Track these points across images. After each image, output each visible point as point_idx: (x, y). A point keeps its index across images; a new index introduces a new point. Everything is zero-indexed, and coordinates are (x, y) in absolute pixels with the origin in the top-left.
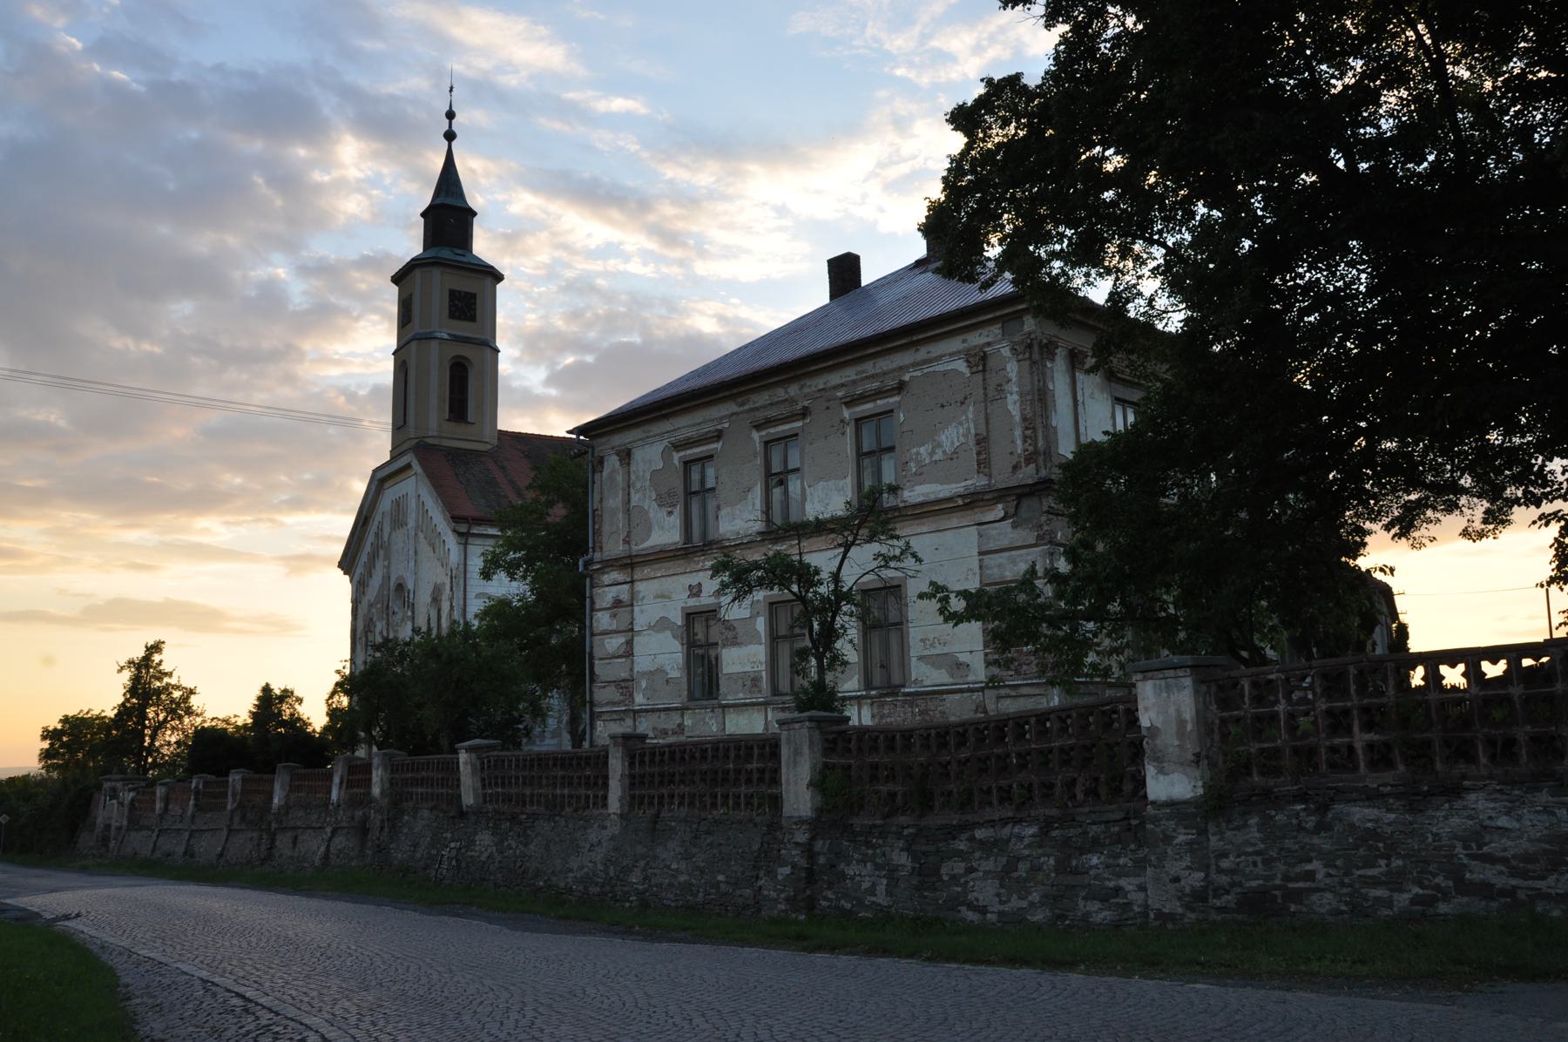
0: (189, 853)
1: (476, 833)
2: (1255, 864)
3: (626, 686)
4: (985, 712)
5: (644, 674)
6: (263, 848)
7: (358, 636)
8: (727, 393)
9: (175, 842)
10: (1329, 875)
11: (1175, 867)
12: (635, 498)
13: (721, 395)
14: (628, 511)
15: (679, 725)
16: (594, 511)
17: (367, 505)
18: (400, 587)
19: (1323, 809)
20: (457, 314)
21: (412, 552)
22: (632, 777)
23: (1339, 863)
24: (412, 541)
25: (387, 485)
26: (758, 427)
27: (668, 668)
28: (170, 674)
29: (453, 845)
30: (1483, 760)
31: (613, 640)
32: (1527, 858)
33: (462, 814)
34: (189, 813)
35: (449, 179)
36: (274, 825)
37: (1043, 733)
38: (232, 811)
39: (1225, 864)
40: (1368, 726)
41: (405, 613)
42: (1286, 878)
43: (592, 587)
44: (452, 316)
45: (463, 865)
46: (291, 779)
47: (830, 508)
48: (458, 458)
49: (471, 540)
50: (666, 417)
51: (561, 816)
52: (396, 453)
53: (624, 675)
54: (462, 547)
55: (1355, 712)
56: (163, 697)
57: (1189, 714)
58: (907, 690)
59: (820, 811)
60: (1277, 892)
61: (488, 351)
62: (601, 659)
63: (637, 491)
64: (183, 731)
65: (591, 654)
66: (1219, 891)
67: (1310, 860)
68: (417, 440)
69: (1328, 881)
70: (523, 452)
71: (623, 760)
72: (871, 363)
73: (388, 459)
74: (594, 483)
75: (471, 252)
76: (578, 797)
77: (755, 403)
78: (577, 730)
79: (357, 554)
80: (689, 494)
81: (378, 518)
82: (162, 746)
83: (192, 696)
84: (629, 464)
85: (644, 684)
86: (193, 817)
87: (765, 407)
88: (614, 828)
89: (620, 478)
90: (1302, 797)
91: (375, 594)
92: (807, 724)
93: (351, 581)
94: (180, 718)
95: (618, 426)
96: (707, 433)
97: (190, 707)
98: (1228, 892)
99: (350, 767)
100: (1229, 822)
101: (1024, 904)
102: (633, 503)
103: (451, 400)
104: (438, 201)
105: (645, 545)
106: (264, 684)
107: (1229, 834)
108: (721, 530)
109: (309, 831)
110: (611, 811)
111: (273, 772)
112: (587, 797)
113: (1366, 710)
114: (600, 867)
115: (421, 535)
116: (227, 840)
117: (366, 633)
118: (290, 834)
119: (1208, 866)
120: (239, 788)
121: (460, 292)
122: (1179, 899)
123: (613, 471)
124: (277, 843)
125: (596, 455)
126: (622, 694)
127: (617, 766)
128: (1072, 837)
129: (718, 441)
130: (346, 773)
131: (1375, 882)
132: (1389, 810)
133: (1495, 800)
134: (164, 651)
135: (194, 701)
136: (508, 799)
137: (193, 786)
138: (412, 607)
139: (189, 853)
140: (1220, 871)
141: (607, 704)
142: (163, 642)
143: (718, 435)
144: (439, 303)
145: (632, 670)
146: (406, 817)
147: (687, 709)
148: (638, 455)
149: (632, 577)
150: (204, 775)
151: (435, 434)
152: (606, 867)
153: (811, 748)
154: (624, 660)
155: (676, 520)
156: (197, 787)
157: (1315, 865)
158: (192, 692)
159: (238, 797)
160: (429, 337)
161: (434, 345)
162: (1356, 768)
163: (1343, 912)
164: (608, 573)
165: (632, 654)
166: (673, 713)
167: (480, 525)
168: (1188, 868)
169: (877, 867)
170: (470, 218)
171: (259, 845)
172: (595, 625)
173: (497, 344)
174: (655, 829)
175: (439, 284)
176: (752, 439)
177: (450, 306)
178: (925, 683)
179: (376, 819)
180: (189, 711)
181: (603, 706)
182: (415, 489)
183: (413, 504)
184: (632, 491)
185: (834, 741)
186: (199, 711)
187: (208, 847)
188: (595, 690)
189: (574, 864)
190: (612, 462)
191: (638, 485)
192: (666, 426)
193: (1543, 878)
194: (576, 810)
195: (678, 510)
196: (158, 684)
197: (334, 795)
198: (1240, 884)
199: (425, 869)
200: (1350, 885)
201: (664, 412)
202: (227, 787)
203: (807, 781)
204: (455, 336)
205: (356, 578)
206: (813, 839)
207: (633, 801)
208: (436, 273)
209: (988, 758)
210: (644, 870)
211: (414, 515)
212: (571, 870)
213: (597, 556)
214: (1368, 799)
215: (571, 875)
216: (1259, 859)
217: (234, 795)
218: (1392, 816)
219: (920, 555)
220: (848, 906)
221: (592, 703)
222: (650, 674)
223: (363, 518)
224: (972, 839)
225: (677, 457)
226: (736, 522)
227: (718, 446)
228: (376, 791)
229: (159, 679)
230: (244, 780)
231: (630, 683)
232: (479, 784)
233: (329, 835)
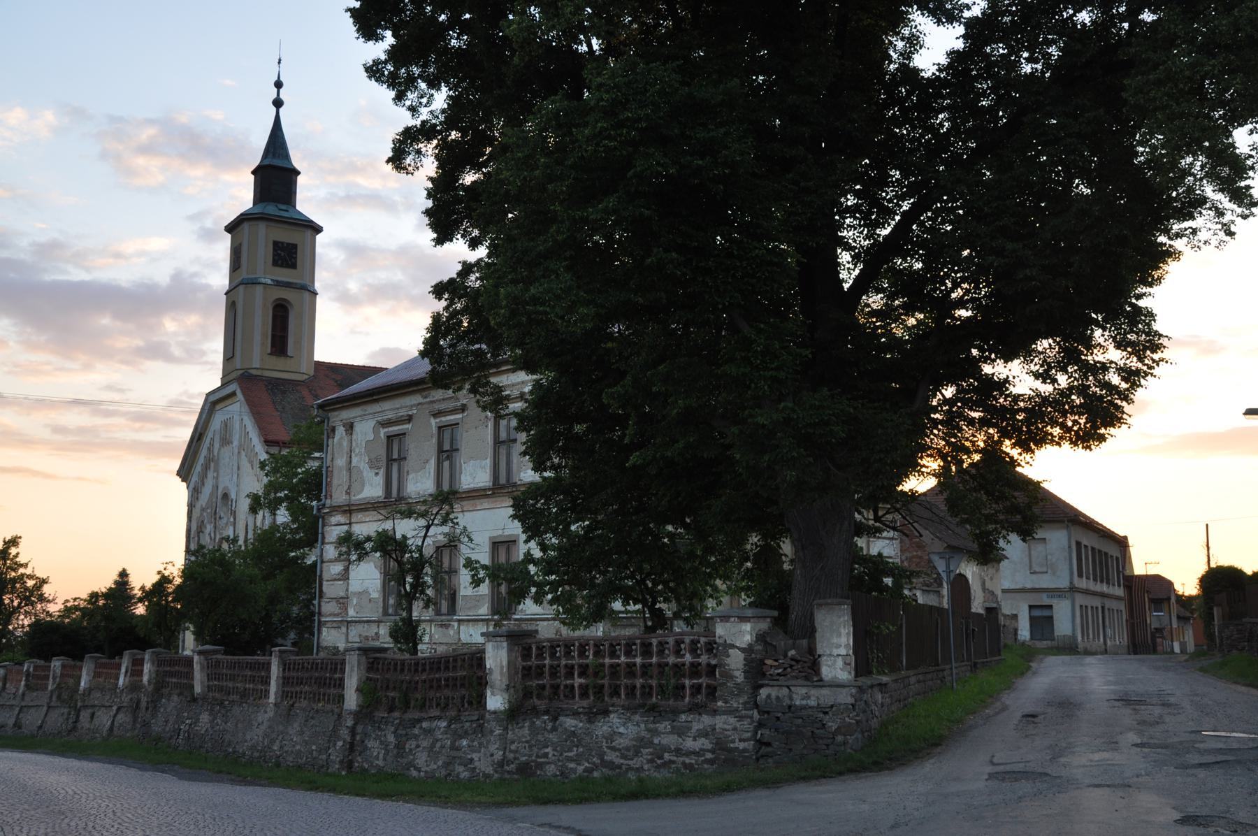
0: (18, 725)
1: (200, 713)
2: (525, 747)
3: (343, 601)
4: (561, 635)
5: (355, 594)
6: (70, 721)
7: (192, 536)
8: (415, 388)
9: (8, 715)
10: (554, 755)
11: (493, 748)
12: (355, 460)
13: (411, 389)
14: (349, 470)
15: (376, 634)
16: (327, 468)
17: (201, 423)
18: (226, 496)
19: (555, 719)
20: (280, 262)
21: (235, 468)
22: (284, 678)
23: (558, 749)
24: (235, 458)
25: (218, 407)
26: (435, 415)
27: (370, 590)
28: (25, 566)
29: (187, 722)
30: (623, 696)
31: (336, 567)
32: (628, 749)
33: (194, 700)
34: (21, 691)
35: (276, 141)
36: (79, 704)
37: (598, 653)
38: (52, 692)
39: (513, 747)
40: (581, 675)
41: (229, 519)
42: (538, 756)
43: (324, 526)
44: (275, 263)
45: (192, 737)
46: (96, 667)
47: (476, 480)
48: (278, 387)
50: (377, 401)
51: (246, 703)
52: (224, 384)
53: (342, 594)
55: (576, 667)
56: (18, 585)
57: (505, 663)
58: (516, 617)
59: (1194, 653)
60: (533, 764)
61: (306, 295)
62: (328, 581)
63: (356, 456)
64: (36, 615)
65: (321, 576)
66: (509, 762)
67: (547, 747)
68: (241, 372)
69: (553, 758)
70: (336, 382)
71: (279, 667)
72: (506, 376)
73: (219, 385)
74: (328, 446)
75: (295, 207)
76: (257, 690)
77: (434, 397)
79: (193, 462)
80: (390, 460)
81: (210, 435)
82: (15, 629)
83: (45, 586)
84: (351, 434)
85: (355, 602)
86: (23, 694)
87: (439, 401)
88: (271, 714)
89: (345, 444)
90: (547, 712)
91: (206, 500)
92: (357, 652)
93: (187, 488)
94: (33, 604)
95: (345, 404)
96: (402, 416)
97: (42, 595)
98: (513, 763)
99: (133, 660)
100: (517, 724)
101: (435, 767)
102: (353, 465)
103: (273, 336)
104: (266, 162)
105: (360, 496)
106: (121, 570)
107: (517, 730)
108: (409, 490)
109: (103, 709)
110: (270, 701)
111: (81, 659)
112: (262, 690)
113: (580, 666)
114: (261, 739)
115: (243, 453)
116: (46, 714)
117: (199, 533)
118: (90, 711)
119: (505, 748)
120: (58, 671)
121: (282, 243)
122: (492, 765)
123: (341, 438)
124: (81, 718)
125: (330, 424)
126: (340, 608)
127: (352, 661)
129: (409, 423)
130: (131, 665)
131: (570, 759)
132: (581, 721)
133: (620, 718)
134: (21, 545)
135: (47, 590)
136: (221, 689)
137: (25, 669)
138: (234, 513)
139: (18, 725)
140: (511, 751)
141: (330, 615)
142: (20, 537)
143: (409, 419)
144: (264, 253)
145: (347, 590)
146: (164, 700)
147: (382, 622)
148: (358, 428)
149: (350, 520)
150: (35, 660)
152: (264, 739)
153: (359, 668)
154: (342, 582)
155: (380, 480)
156: (28, 670)
157: (549, 750)
158: (44, 581)
159: (58, 680)
160: (254, 282)
161: (259, 289)
162: (574, 697)
163: (557, 776)
164: (334, 516)
165: (348, 579)
166: (373, 624)
168: (497, 749)
169: (381, 743)
170: (294, 177)
171: (67, 719)
172: (324, 554)
173: (316, 288)
174: (289, 715)
175: (264, 236)
176: (430, 424)
177: (274, 255)
178: (527, 612)
179: (144, 700)
180: (42, 598)
181: (326, 617)
182: (237, 412)
183: (237, 426)
184: (353, 455)
185: (373, 663)
186: (51, 598)
187: (32, 720)
188: (323, 604)
189: (248, 738)
190: (340, 431)
191: (357, 450)
192: (376, 407)
193: (632, 759)
194: (254, 700)
195: (382, 472)
196: (13, 574)
197: (121, 682)
198: (518, 759)
199: (170, 739)
200: (562, 761)
201: (374, 397)
202: (50, 671)
203: (355, 688)
204: (277, 281)
205: (192, 485)
206: (355, 724)
207: (284, 695)
208: (262, 227)
209: (433, 680)
210: (281, 741)
211: (237, 436)
212: (246, 741)
213: (328, 502)
214: (574, 714)
215: (246, 744)
216: (527, 745)
217: (54, 678)
218: (581, 724)
219: (473, 537)
220: (366, 766)
221: (320, 613)
222: (359, 594)
223: (198, 434)
224: (421, 728)
225: (383, 432)
226: (418, 484)
227: (408, 426)
228: (145, 679)
229: (15, 570)
230: (63, 666)
231: (346, 600)
232: (206, 678)
233: (115, 712)
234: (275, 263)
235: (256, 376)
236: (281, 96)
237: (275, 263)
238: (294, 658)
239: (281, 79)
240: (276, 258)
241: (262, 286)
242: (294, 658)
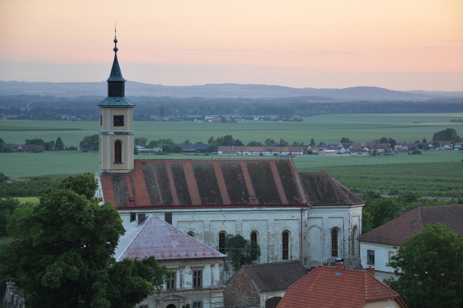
20: (117, 124)
121: (117, 116)
177: (114, 122)
234: (115, 125)
235: (109, 173)
236: (117, 47)
237: (115, 125)
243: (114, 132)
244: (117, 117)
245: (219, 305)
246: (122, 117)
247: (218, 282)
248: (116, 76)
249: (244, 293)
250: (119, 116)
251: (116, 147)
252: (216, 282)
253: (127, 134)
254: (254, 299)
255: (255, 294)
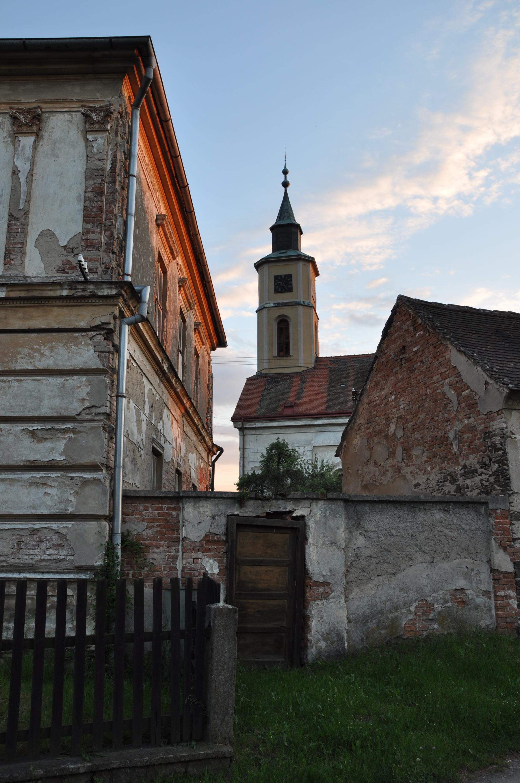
20: (280, 290)
49: (246, 432)
54: (242, 436)
78: (344, 647)
104: (280, 223)
121: (281, 276)
128: (236, 683)
151: (267, 367)
167: (250, 421)
177: (275, 286)
204: (278, 304)
234: (276, 291)
235: (265, 374)
236: (288, 179)
237: (276, 291)
238: (73, 766)
239: (287, 168)
240: (277, 287)
241: (267, 309)
242: (73, 766)
243: (274, 304)
244: (279, 278)
245: (61, 445)
246: (290, 276)
247: (69, 249)
248: (283, 219)
249: (416, 451)
250: (283, 277)
251: (279, 330)
252: (43, 255)
253: (297, 304)
254: (469, 472)
255: (472, 429)
